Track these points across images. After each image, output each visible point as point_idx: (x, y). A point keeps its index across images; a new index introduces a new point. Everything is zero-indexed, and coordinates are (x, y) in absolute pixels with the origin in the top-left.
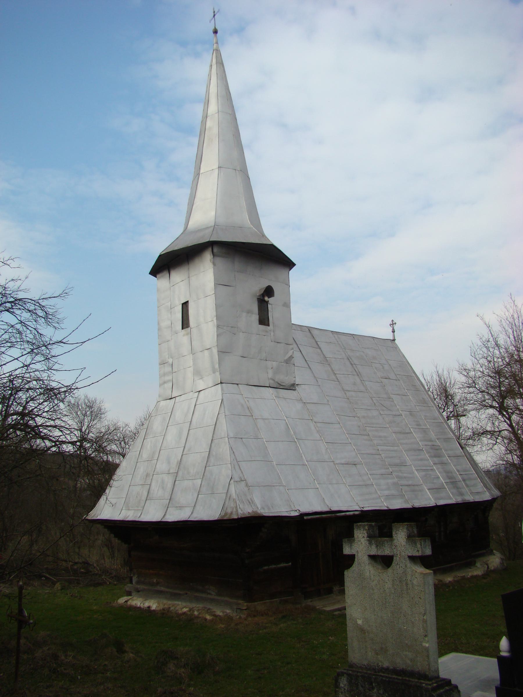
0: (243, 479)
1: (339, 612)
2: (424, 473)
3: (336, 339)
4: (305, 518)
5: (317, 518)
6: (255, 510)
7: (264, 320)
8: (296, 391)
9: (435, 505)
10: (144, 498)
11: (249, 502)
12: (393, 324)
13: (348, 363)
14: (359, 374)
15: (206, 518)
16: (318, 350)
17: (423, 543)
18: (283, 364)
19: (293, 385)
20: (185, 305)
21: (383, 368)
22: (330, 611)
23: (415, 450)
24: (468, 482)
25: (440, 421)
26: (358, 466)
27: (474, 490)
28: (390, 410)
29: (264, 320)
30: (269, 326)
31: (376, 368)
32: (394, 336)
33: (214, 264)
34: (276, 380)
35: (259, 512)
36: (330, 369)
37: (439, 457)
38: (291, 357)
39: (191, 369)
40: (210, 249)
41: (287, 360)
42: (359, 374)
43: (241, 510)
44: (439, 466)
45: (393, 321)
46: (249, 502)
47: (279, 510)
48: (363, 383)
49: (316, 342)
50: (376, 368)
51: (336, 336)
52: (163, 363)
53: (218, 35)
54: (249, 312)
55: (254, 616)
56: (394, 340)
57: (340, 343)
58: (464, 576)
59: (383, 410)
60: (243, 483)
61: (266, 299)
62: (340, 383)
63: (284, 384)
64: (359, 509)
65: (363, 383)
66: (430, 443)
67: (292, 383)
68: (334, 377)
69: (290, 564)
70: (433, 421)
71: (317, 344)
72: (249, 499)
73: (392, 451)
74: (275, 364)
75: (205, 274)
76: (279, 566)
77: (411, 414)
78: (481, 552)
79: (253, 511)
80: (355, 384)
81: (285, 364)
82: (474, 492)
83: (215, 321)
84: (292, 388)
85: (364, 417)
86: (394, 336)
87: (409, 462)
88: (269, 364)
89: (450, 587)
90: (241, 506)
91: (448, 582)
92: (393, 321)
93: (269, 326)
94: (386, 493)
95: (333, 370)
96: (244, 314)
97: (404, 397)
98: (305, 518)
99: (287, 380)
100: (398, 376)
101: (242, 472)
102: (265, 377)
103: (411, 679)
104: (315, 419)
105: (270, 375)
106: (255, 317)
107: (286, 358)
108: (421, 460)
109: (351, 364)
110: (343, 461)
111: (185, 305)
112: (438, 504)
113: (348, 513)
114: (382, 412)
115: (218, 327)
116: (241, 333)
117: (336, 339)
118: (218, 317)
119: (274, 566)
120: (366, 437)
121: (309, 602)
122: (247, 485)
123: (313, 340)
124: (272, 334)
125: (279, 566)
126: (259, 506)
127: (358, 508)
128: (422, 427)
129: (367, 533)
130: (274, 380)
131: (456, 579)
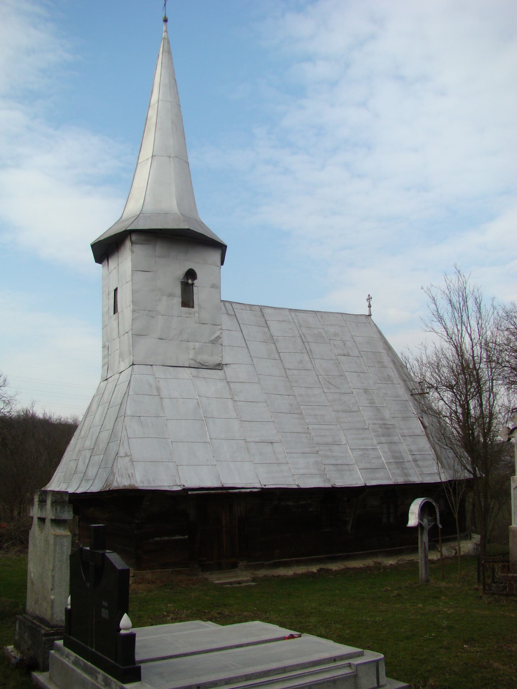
0: (128, 454)
1: (229, 585)
2: (360, 453)
3: (292, 317)
4: (190, 493)
5: (199, 494)
6: (132, 484)
7: (187, 301)
8: (222, 371)
9: (363, 485)
10: (73, 473)
11: (129, 476)
12: (369, 299)
13: (299, 341)
14: (309, 353)
15: (94, 491)
16: (266, 329)
18: (207, 344)
20: (116, 290)
21: (345, 344)
22: (219, 583)
23: (357, 429)
24: (420, 463)
26: (275, 444)
27: (425, 471)
29: (187, 301)
31: (334, 345)
32: (370, 311)
33: (132, 252)
34: (198, 360)
35: (136, 485)
36: (273, 347)
37: (389, 436)
38: (219, 337)
39: (118, 352)
40: (129, 237)
41: (213, 340)
42: (309, 353)
43: (118, 483)
44: (385, 446)
45: (369, 295)
46: (129, 476)
47: (160, 485)
50: (334, 345)
51: (293, 314)
52: (104, 347)
53: (168, 23)
54: (171, 295)
55: (140, 583)
56: (370, 315)
59: (329, 388)
60: (128, 459)
61: (190, 281)
62: (282, 362)
63: (207, 364)
64: (261, 487)
66: (380, 422)
67: (218, 362)
69: (187, 537)
70: (394, 399)
71: (266, 322)
73: (326, 430)
74: (197, 345)
75: (126, 260)
76: (173, 538)
77: (365, 392)
78: (452, 536)
80: (301, 362)
81: (210, 345)
82: (425, 473)
83: (132, 306)
84: (217, 367)
85: (301, 395)
86: (370, 311)
88: (191, 345)
89: (381, 569)
90: (118, 480)
91: (388, 565)
92: (369, 295)
94: (302, 471)
96: (165, 298)
98: (190, 493)
99: (215, 360)
100: (362, 353)
101: (130, 448)
102: (185, 358)
103: (41, 625)
104: (236, 398)
105: (191, 356)
106: (178, 300)
108: (363, 439)
109: (303, 342)
110: (257, 440)
111: (116, 290)
112: (367, 485)
113: (243, 490)
114: (326, 390)
115: (134, 311)
117: (292, 317)
119: (166, 538)
120: (297, 416)
121: (207, 575)
122: (132, 461)
124: (197, 315)
125: (173, 538)
126: (138, 480)
127: (258, 486)
129: (39, 498)
130: (195, 361)
131: (400, 562)
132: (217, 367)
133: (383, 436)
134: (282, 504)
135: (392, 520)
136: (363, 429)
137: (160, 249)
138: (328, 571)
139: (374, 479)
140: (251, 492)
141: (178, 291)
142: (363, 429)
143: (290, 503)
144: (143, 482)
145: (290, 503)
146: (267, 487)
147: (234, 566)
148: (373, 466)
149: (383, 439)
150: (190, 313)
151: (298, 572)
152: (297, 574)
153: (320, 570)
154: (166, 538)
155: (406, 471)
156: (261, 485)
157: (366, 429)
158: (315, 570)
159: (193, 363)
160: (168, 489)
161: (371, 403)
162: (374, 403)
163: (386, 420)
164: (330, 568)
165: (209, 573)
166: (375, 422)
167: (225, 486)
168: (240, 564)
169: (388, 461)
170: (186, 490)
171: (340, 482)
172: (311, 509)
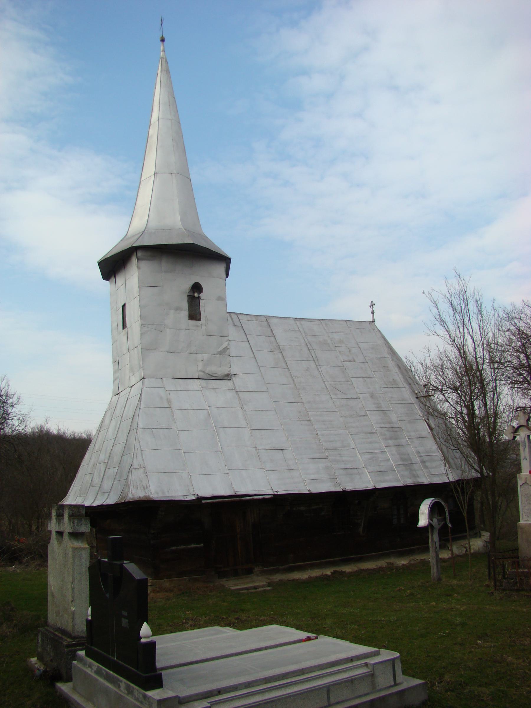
4: (203, 502)
5: (218, 502)
6: (147, 495)
7: (194, 314)
8: (231, 381)
11: (144, 488)
13: (305, 349)
14: (316, 360)
17: (76, 522)
19: (228, 375)
20: (124, 306)
21: (350, 351)
25: (410, 402)
26: (285, 451)
27: (434, 471)
28: (344, 394)
29: (194, 314)
30: (200, 320)
31: (340, 352)
32: (373, 317)
33: (139, 268)
34: (207, 372)
35: (151, 496)
38: (226, 348)
39: (128, 366)
41: (221, 351)
42: (316, 360)
44: (393, 449)
45: (372, 302)
46: (144, 488)
48: (318, 368)
49: (272, 330)
50: (340, 352)
51: (298, 323)
52: (114, 362)
53: (165, 43)
55: (158, 592)
56: (373, 321)
57: (301, 329)
58: (424, 559)
60: (142, 471)
61: (196, 295)
63: (216, 375)
65: (318, 368)
66: (388, 426)
67: (226, 373)
68: (284, 365)
69: (202, 545)
70: (400, 402)
71: (272, 332)
72: (145, 486)
74: (206, 356)
75: (133, 276)
76: (189, 546)
77: (372, 397)
79: (145, 496)
80: (307, 370)
84: (226, 378)
85: (309, 402)
86: (373, 317)
87: (353, 446)
88: (200, 357)
89: (393, 570)
90: (133, 491)
91: (401, 565)
92: (372, 302)
93: (200, 320)
94: (313, 477)
95: (284, 358)
96: (172, 312)
97: (368, 380)
98: (203, 502)
101: (143, 460)
102: (194, 370)
104: (245, 407)
105: (200, 368)
106: (185, 313)
107: (221, 349)
108: (371, 443)
109: (309, 350)
111: (124, 306)
113: (255, 497)
114: (333, 397)
115: (142, 326)
116: (168, 330)
118: (142, 317)
119: (182, 547)
120: (306, 422)
122: (146, 473)
123: (269, 329)
124: (204, 327)
125: (189, 546)
126: (153, 492)
127: (271, 492)
128: (382, 409)
130: (204, 372)
131: (412, 562)
132: (226, 378)
133: (391, 439)
134: (294, 509)
135: (402, 521)
136: (371, 433)
137: (165, 264)
138: (342, 573)
139: (384, 482)
140: (253, 500)
141: (185, 304)
142: (371, 433)
143: (302, 508)
144: (157, 493)
145: (302, 508)
146: (279, 493)
147: (249, 572)
148: (382, 469)
149: (391, 442)
150: (198, 326)
151: (312, 576)
152: (311, 577)
153: (334, 573)
154: (182, 547)
155: (414, 472)
156: (273, 491)
157: (374, 433)
158: (329, 573)
159: (202, 375)
160: (182, 499)
161: (378, 407)
162: (380, 407)
163: (392, 423)
164: (343, 570)
165: (225, 579)
166: (383, 425)
167: (238, 493)
168: (256, 569)
169: (396, 464)
170: (200, 499)
171: (350, 487)
172: (323, 514)
